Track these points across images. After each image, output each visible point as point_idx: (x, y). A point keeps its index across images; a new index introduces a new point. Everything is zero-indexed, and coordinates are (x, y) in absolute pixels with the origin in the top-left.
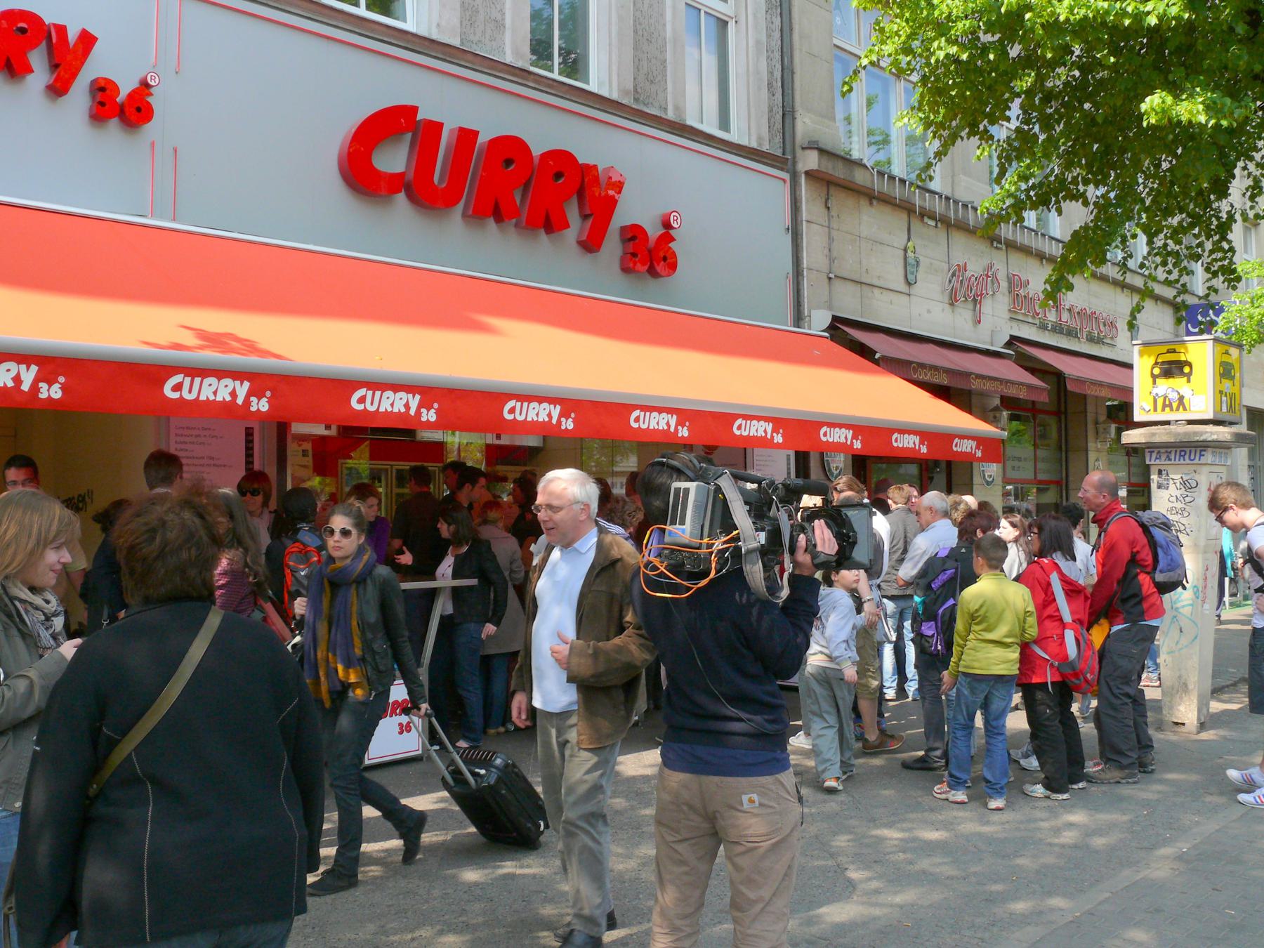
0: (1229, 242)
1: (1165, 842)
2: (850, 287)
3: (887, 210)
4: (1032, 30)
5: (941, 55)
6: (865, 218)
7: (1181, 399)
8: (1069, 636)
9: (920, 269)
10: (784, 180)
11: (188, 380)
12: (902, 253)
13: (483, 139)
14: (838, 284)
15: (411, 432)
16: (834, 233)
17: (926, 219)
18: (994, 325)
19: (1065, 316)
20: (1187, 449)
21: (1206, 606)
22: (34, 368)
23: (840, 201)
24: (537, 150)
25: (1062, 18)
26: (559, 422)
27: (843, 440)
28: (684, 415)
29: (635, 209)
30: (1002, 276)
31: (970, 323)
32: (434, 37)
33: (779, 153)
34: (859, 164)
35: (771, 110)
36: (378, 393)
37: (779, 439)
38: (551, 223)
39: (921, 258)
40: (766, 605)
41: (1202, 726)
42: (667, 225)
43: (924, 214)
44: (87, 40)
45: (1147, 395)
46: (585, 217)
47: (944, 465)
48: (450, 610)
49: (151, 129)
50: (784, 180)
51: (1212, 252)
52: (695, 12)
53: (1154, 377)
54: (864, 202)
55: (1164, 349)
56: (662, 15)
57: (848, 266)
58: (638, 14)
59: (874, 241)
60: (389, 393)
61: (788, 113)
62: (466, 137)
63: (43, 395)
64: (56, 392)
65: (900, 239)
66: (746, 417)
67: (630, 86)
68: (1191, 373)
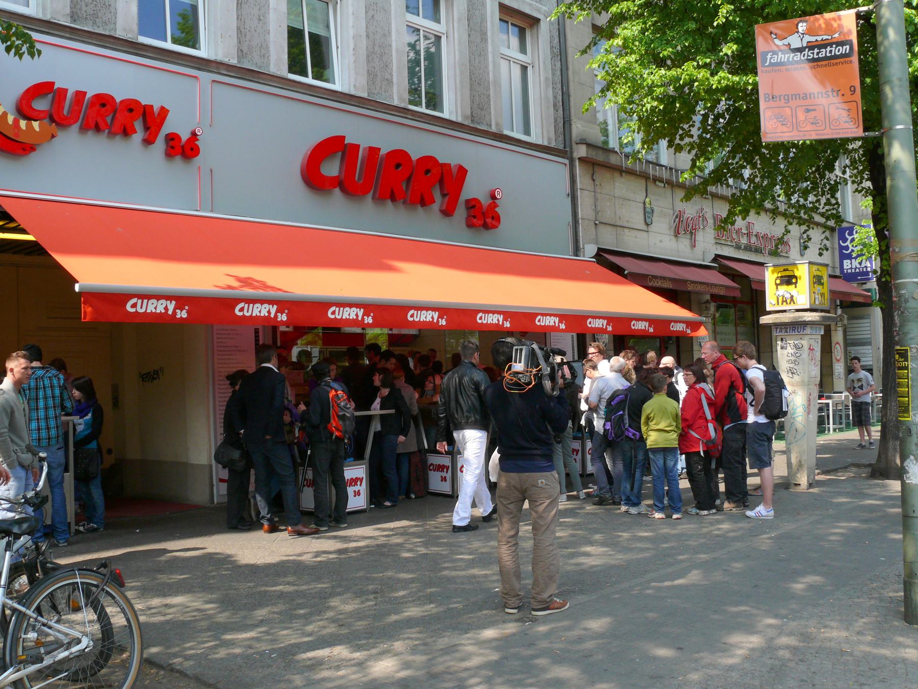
0: (836, 199)
1: (765, 533)
2: (609, 229)
3: (632, 178)
4: (699, 93)
5: (649, 106)
6: (617, 184)
7: (792, 297)
8: (711, 426)
9: (655, 215)
10: (565, 165)
11: (140, 301)
12: (642, 205)
13: (383, 152)
14: (601, 227)
15: (339, 329)
16: (598, 196)
17: (657, 183)
18: (706, 246)
19: (753, 239)
20: (797, 326)
21: (810, 416)
22: (174, 302)
23: (603, 176)
24: (415, 156)
25: (714, 87)
26: (438, 321)
27: (601, 326)
28: (507, 314)
29: (474, 188)
30: (709, 216)
31: (689, 247)
32: (352, 93)
33: (561, 147)
34: (613, 151)
35: (556, 121)
36: (251, 305)
37: (563, 326)
38: (424, 201)
39: (655, 208)
40: (551, 397)
41: (810, 485)
42: (493, 197)
43: (656, 180)
44: (164, 112)
45: (773, 294)
46: (444, 195)
47: (674, 339)
48: (379, 428)
49: (198, 160)
50: (565, 165)
51: (825, 204)
52: (507, 62)
53: (777, 285)
54: (617, 175)
55: (782, 268)
56: (487, 67)
57: (607, 216)
58: (472, 68)
59: (624, 200)
60: (258, 305)
61: (567, 123)
62: (373, 151)
63: (178, 316)
64: (184, 314)
65: (641, 196)
66: (543, 315)
67: (468, 113)
68: (796, 283)
